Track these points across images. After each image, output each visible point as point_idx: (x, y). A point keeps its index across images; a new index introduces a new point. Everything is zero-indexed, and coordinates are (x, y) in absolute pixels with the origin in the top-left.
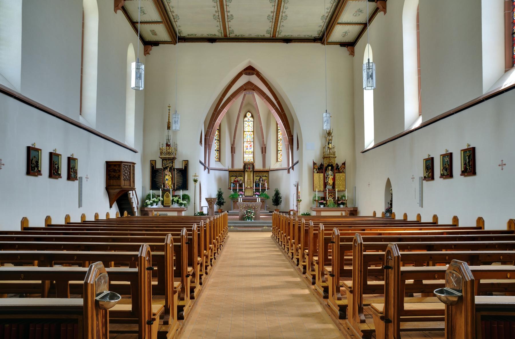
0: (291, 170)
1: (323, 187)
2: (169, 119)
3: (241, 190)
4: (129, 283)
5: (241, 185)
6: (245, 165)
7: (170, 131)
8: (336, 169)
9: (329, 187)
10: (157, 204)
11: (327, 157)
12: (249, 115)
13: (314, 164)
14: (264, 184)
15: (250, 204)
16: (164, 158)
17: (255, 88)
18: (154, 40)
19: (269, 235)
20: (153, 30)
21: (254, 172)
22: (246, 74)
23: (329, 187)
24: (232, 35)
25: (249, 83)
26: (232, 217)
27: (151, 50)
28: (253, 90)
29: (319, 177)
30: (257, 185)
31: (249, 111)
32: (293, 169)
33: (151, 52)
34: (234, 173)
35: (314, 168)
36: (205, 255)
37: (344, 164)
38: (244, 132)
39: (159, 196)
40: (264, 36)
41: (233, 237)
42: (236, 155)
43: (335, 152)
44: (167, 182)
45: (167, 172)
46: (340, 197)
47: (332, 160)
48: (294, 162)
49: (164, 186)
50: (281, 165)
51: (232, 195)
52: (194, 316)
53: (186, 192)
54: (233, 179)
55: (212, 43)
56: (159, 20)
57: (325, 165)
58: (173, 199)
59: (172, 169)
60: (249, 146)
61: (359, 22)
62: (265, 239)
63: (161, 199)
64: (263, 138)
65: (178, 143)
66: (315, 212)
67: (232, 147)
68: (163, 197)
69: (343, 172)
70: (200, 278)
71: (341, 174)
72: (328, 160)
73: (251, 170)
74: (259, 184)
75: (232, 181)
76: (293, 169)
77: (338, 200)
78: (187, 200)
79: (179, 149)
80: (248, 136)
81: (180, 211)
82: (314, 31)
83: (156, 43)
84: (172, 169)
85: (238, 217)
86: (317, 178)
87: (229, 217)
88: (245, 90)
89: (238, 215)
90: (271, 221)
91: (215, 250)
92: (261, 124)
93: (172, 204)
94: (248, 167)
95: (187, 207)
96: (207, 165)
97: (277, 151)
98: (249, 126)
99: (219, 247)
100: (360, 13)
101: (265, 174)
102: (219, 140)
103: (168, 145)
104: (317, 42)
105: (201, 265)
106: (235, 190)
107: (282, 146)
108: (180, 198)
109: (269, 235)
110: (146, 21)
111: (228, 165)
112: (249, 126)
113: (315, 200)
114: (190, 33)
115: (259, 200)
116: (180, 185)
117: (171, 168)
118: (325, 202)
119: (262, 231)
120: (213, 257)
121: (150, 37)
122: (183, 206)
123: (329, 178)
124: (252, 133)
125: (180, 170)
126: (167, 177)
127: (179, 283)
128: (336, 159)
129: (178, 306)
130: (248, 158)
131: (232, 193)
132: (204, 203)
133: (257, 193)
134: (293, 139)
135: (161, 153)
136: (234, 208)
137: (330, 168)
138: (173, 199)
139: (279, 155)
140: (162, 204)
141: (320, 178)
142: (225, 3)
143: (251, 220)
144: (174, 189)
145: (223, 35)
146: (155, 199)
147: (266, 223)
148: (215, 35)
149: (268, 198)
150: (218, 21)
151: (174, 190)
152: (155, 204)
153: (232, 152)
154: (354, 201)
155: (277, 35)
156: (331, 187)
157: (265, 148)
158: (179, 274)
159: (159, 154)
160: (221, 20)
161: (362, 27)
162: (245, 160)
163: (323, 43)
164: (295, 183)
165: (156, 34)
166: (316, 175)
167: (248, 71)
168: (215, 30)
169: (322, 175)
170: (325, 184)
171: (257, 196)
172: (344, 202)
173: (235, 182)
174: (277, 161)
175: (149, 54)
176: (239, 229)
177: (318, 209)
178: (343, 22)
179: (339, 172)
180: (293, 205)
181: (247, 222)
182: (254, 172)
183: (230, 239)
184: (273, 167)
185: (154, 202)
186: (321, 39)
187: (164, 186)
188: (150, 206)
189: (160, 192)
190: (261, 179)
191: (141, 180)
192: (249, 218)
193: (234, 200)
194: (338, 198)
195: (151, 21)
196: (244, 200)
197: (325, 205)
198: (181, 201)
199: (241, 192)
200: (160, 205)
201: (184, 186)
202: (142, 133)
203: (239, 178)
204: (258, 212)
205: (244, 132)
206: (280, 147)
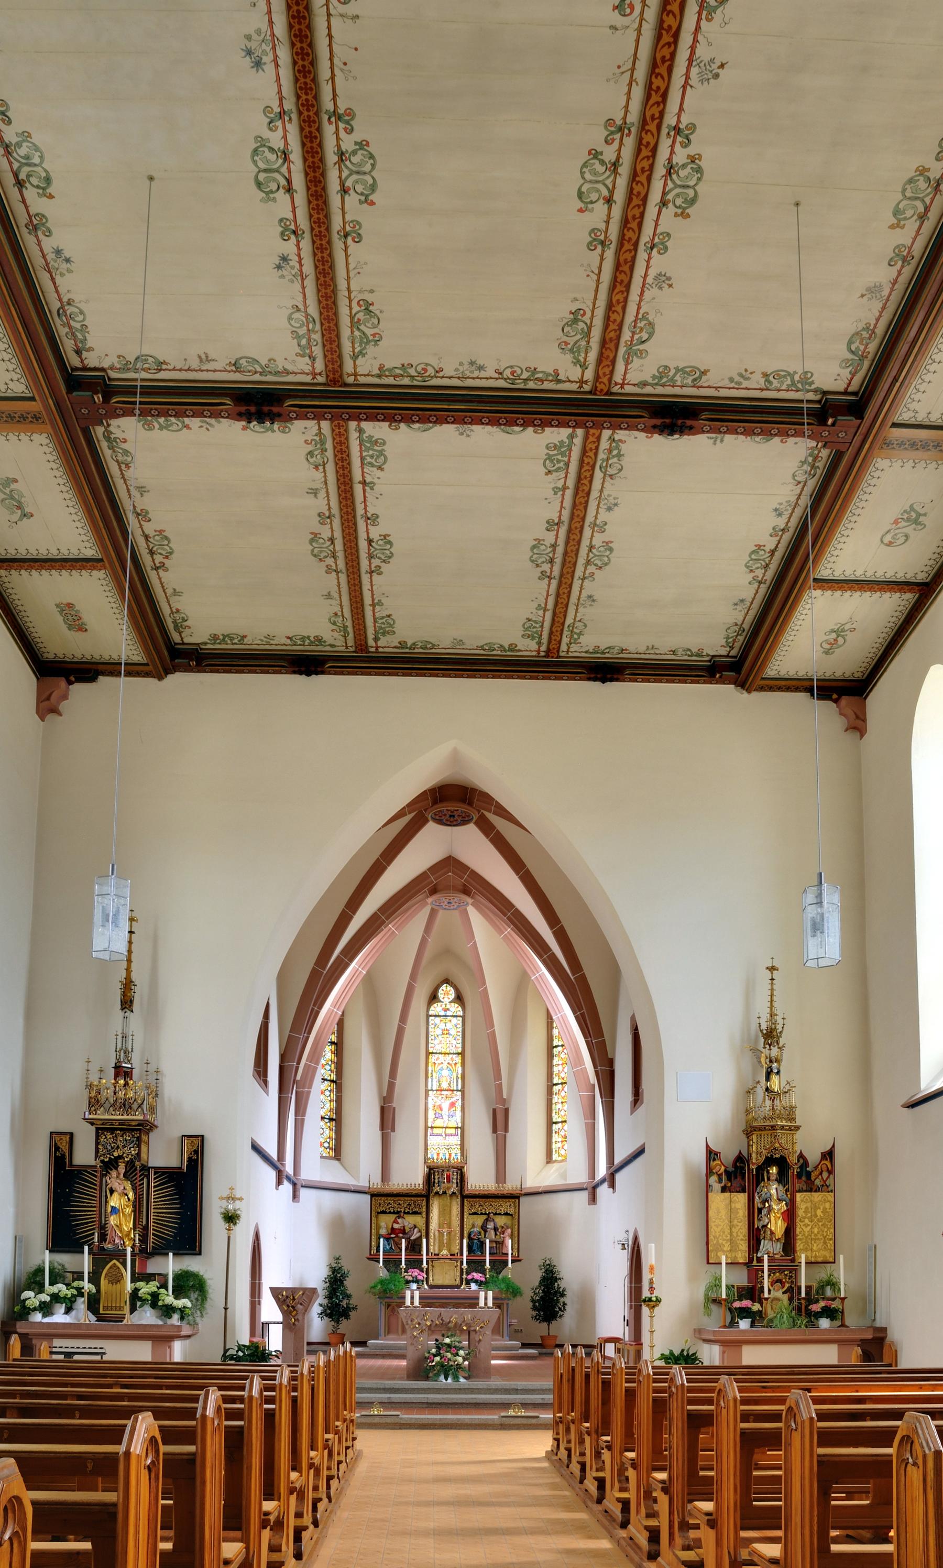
0: (603, 1190)
1: (743, 1246)
2: (128, 970)
3: (414, 1263)
4: (87, 1546)
5: (414, 1247)
6: (432, 1172)
7: (135, 1019)
8: (799, 1176)
9: (770, 1248)
10: (68, 1311)
11: (762, 1129)
12: (447, 993)
13: (712, 1155)
14: (500, 1244)
15: (453, 1315)
16: (105, 1121)
17: (471, 885)
18: (78, 656)
19: (539, 1445)
20: (70, 605)
21: (463, 1197)
22: (440, 822)
23: (770, 1248)
24: (388, 644)
25: (450, 864)
26: (380, 1362)
27: (65, 697)
28: (466, 891)
29: (729, 1208)
30: (476, 1246)
31: (447, 981)
32: (612, 1185)
33: (64, 706)
34: (390, 1200)
35: (709, 1172)
36: (292, 1491)
37: (829, 1155)
39: (79, 1276)
40: (512, 647)
41: (380, 1453)
42: (399, 1139)
43: (792, 1108)
44: (113, 1220)
45: (116, 1180)
46: (815, 1285)
47: (783, 1139)
48: (618, 1160)
49: (103, 1237)
50: (564, 1175)
51: (382, 1282)
52: (344, 1501)
53: (191, 1264)
54: (386, 1222)
55: (308, 674)
56: (90, 552)
57: (756, 1160)
58: (136, 1291)
59: (136, 1171)
60: (446, 1105)
61: (900, 577)
62: (519, 1473)
63: (87, 1286)
64: (498, 1076)
65: (167, 1067)
66: (716, 1349)
67: (383, 1110)
68: (95, 1278)
69: (825, 1187)
70: (298, 1539)
71: (817, 1196)
72: (767, 1140)
73: (454, 1188)
74: (482, 1244)
75: (383, 1231)
76: (612, 1185)
77: (810, 1300)
78: (194, 1295)
79: (171, 1089)
80: (445, 1071)
81: (162, 1339)
82: (713, 642)
83: (87, 671)
84: (136, 1171)
85: (404, 1363)
86: (723, 1213)
87: (360, 1362)
88: (434, 891)
89: (402, 1357)
90: (549, 1383)
91: (299, 1515)
92: (492, 1025)
93: (133, 1309)
94: (442, 1180)
95: (194, 1324)
96: (289, 1168)
97: (550, 1123)
98: (446, 1032)
99: (315, 1506)
100: (909, 530)
101: (505, 1206)
102: (338, 1083)
103: (121, 1072)
104: (722, 681)
105: (301, 1495)
106: (392, 1263)
107: (567, 1106)
108: (164, 1286)
109: (539, 1445)
110: (33, 554)
111: (365, 1169)
112: (446, 1032)
113: (717, 1301)
114: (220, 629)
115: (486, 1298)
116: (169, 1233)
117: (130, 1165)
118: (756, 1307)
119: (502, 1427)
120: (307, 1520)
121: (59, 642)
122: (175, 1319)
123: (770, 1209)
124: (458, 1059)
125: (168, 1175)
126: (114, 1201)
127: (240, 1545)
128: (798, 1136)
129: (268, 1563)
130: (443, 1148)
131: (383, 1273)
132: (270, 1311)
133: (477, 1276)
134: (612, 1074)
135: (94, 1103)
136: (389, 1331)
137: (774, 1170)
138: (136, 1291)
139: (555, 1138)
140: (93, 1304)
141: (732, 1211)
142: (357, 475)
143: (456, 1378)
144: (143, 1251)
145: (351, 642)
146: (60, 1288)
147: (516, 1391)
148: (319, 640)
149: (515, 1292)
150: (329, 570)
151: (144, 1252)
152: (61, 1308)
153: (383, 1127)
154: (868, 1301)
155: (564, 647)
156: (778, 1247)
157: (506, 1111)
158: (235, 1519)
159: (85, 1107)
160: (341, 564)
161: (909, 597)
162: (432, 1154)
163: (743, 684)
164: (622, 1237)
165: (82, 629)
166: (719, 1200)
167: (445, 807)
168: (314, 618)
169: (741, 1199)
170: (755, 1236)
171: (474, 1286)
172: (835, 1305)
173: (394, 1235)
174: (549, 1159)
175: (55, 711)
176: (406, 1416)
177: (730, 1334)
178: (838, 575)
179: (811, 1188)
180: (611, 1319)
181: (439, 1389)
182: (465, 1197)
183: (362, 1468)
184: (531, 1182)
185: (56, 1298)
186: (740, 665)
187: (103, 1237)
188: (37, 1317)
189: (85, 1262)
190: (490, 1225)
191: (11, 1210)
192: (446, 1370)
193: (389, 1298)
194: (809, 1288)
195: (54, 553)
196: (426, 1301)
197: (756, 1318)
198: (168, 1298)
199: (416, 1272)
200: (81, 1314)
201: (187, 1239)
202: (20, 1022)
203: (409, 1221)
204: (482, 1348)
205: (428, 1054)
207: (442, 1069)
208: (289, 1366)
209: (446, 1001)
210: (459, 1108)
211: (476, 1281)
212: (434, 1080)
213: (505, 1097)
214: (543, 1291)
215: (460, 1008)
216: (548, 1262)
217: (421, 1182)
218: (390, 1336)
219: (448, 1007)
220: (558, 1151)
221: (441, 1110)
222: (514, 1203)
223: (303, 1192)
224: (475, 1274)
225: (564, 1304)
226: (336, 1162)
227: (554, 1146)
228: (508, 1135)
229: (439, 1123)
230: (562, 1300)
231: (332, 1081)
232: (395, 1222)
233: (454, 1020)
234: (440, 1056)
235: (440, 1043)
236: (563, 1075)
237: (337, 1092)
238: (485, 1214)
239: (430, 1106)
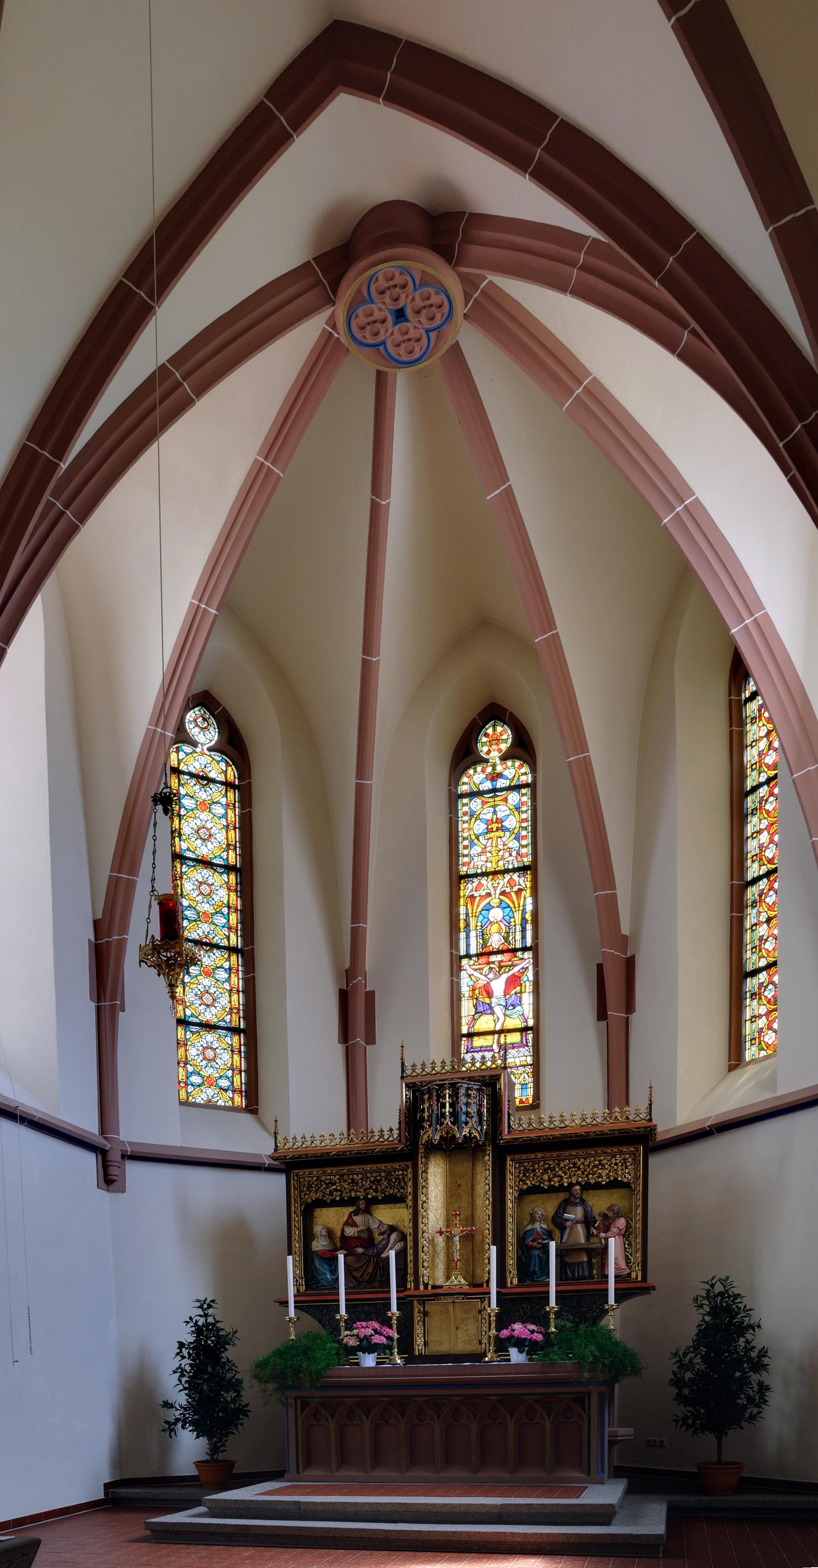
12: (496, 740)
34: (331, 1173)
38: (534, 949)
60: (498, 986)
67: (344, 998)
92: (581, 744)
97: (739, 973)
98: (497, 826)
139: (752, 1007)
153: (345, 1034)
157: (630, 964)
174: (735, 1057)
184: (683, 1111)
205: (457, 879)
206: (764, 936)
207: (488, 908)
208: (298, 1472)
209: (495, 755)
210: (529, 987)
211: (520, 1344)
212: (473, 934)
213: (625, 930)
214: (705, 1359)
215: (525, 769)
216: (719, 1288)
217: (395, 1126)
218: (309, 1473)
219: (499, 769)
220: (757, 1039)
221: (490, 994)
222: (634, 1155)
223: (134, 1171)
224: (517, 1327)
225: (764, 1389)
226: (248, 1118)
227: (748, 1029)
228: (634, 1018)
229: (485, 1023)
230: (754, 1377)
231: (231, 950)
232: (349, 1223)
233: (514, 798)
234: (484, 881)
235: (484, 852)
236: (770, 1038)
237: (245, 972)
238: (561, 1189)
239: (465, 990)
